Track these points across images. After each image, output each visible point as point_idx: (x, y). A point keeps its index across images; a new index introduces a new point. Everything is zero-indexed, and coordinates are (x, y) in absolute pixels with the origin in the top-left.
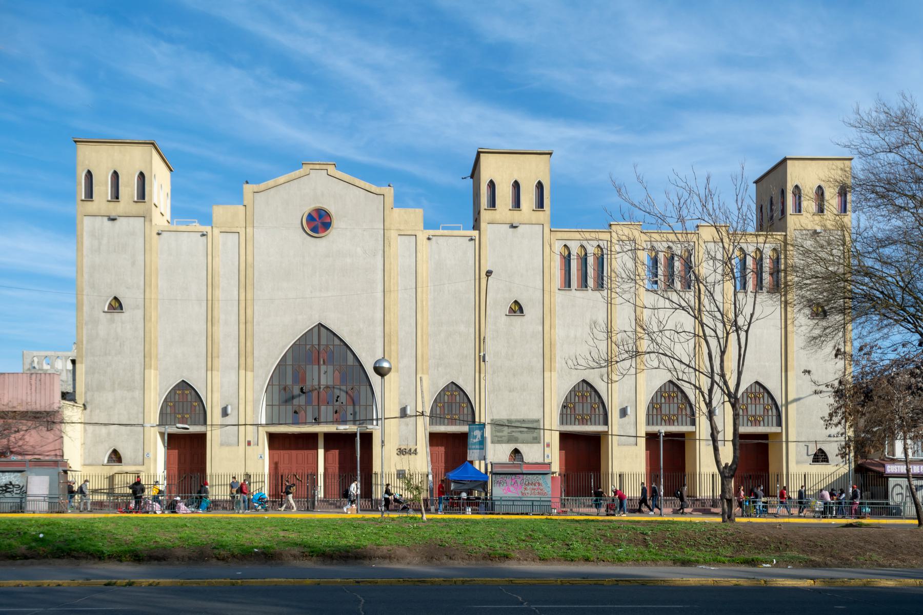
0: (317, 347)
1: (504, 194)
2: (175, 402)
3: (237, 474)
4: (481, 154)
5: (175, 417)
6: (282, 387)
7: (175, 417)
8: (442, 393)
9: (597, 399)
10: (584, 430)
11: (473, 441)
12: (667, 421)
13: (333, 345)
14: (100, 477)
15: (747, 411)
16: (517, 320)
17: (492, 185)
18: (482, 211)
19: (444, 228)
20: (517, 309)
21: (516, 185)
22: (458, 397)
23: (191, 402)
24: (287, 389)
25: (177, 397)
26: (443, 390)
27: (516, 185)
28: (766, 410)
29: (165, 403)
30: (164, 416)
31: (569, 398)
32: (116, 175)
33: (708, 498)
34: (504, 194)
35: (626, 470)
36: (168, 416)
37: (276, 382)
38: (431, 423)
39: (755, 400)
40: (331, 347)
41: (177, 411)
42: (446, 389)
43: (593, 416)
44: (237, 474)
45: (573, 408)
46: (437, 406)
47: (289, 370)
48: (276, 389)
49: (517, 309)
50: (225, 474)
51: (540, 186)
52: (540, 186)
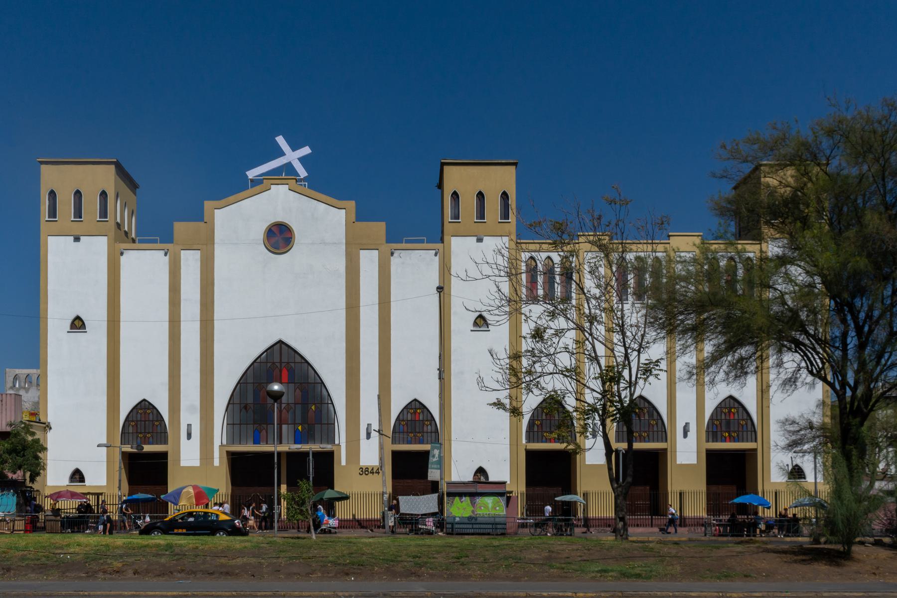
0: (278, 365)
1: (468, 204)
2: (721, 420)
3: (351, 493)
4: (445, 167)
5: (137, 437)
6: (243, 406)
7: (137, 437)
8: (405, 411)
9: (745, 414)
10: (262, 450)
11: (433, 460)
12: (638, 438)
13: (267, 363)
14: (112, 497)
15: (747, 427)
16: (79, 336)
17: (455, 195)
18: (446, 223)
19: (407, 242)
20: (78, 324)
21: (480, 195)
22: (151, 414)
23: (423, 421)
24: (248, 407)
25: (139, 416)
26: (406, 407)
27: (480, 195)
28: (740, 425)
29: (397, 421)
30: (621, 433)
31: (715, 415)
32: (78, 194)
33: (602, 518)
34: (468, 204)
35: (685, 488)
36: (131, 435)
37: (237, 400)
38: (394, 441)
39: (730, 415)
40: (293, 365)
41: (139, 431)
42: (723, 405)
43: (651, 433)
44: (351, 493)
45: (719, 426)
46: (129, 424)
47: (250, 388)
48: (237, 407)
49: (78, 324)
50: (602, 492)
51: (505, 196)
52: (505, 196)
